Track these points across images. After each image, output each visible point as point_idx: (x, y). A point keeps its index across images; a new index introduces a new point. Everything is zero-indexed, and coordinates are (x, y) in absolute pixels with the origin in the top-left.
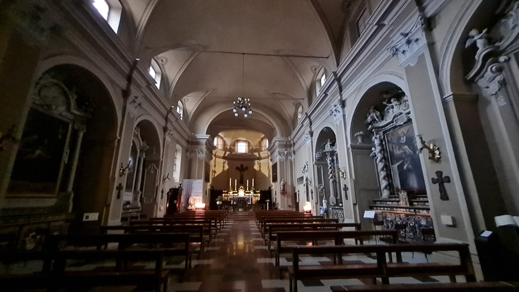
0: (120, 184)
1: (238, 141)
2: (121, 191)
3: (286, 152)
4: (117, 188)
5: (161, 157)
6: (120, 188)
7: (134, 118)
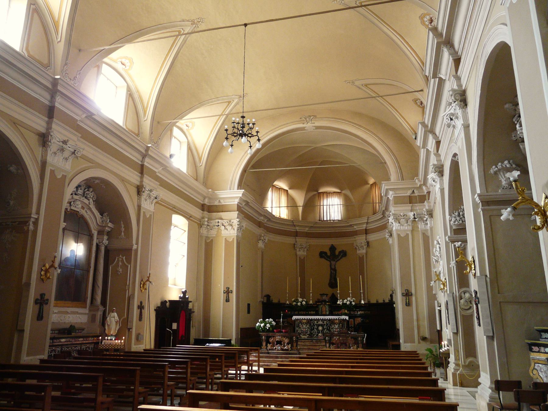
0: (42, 295)
1: (321, 195)
2: (45, 307)
3: (411, 215)
4: (36, 302)
5: (134, 242)
6: (41, 301)
7: (64, 177)
